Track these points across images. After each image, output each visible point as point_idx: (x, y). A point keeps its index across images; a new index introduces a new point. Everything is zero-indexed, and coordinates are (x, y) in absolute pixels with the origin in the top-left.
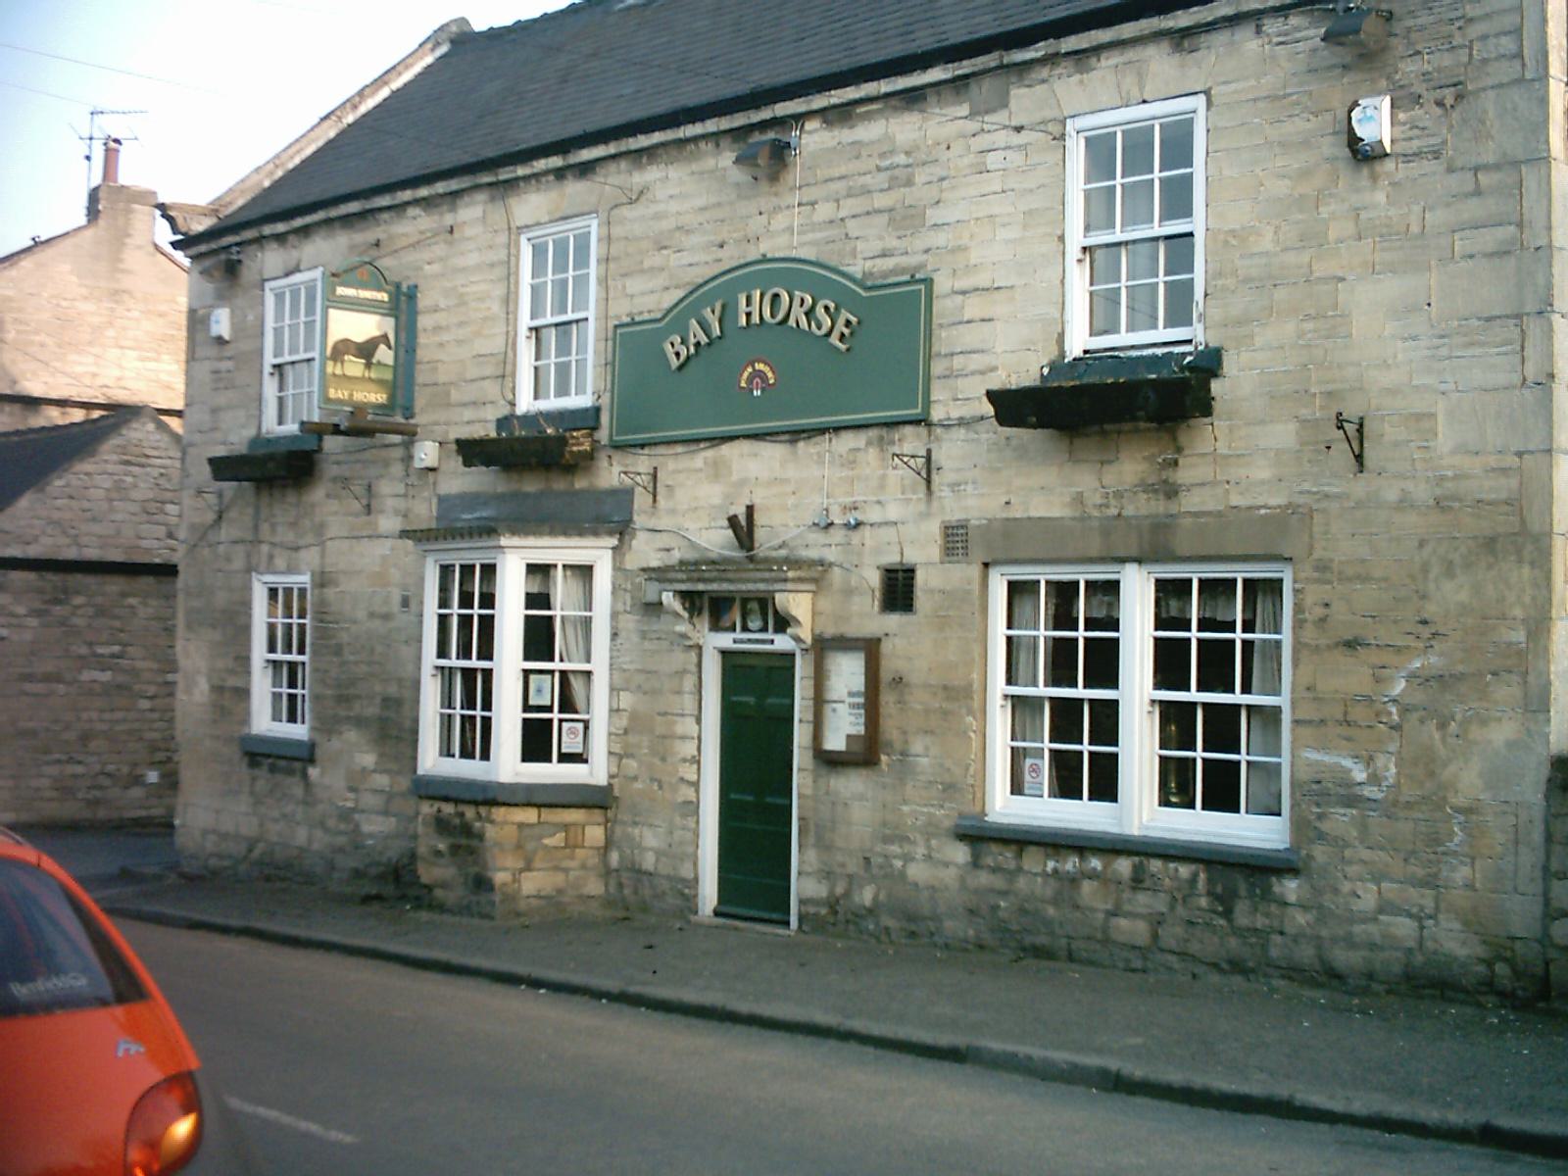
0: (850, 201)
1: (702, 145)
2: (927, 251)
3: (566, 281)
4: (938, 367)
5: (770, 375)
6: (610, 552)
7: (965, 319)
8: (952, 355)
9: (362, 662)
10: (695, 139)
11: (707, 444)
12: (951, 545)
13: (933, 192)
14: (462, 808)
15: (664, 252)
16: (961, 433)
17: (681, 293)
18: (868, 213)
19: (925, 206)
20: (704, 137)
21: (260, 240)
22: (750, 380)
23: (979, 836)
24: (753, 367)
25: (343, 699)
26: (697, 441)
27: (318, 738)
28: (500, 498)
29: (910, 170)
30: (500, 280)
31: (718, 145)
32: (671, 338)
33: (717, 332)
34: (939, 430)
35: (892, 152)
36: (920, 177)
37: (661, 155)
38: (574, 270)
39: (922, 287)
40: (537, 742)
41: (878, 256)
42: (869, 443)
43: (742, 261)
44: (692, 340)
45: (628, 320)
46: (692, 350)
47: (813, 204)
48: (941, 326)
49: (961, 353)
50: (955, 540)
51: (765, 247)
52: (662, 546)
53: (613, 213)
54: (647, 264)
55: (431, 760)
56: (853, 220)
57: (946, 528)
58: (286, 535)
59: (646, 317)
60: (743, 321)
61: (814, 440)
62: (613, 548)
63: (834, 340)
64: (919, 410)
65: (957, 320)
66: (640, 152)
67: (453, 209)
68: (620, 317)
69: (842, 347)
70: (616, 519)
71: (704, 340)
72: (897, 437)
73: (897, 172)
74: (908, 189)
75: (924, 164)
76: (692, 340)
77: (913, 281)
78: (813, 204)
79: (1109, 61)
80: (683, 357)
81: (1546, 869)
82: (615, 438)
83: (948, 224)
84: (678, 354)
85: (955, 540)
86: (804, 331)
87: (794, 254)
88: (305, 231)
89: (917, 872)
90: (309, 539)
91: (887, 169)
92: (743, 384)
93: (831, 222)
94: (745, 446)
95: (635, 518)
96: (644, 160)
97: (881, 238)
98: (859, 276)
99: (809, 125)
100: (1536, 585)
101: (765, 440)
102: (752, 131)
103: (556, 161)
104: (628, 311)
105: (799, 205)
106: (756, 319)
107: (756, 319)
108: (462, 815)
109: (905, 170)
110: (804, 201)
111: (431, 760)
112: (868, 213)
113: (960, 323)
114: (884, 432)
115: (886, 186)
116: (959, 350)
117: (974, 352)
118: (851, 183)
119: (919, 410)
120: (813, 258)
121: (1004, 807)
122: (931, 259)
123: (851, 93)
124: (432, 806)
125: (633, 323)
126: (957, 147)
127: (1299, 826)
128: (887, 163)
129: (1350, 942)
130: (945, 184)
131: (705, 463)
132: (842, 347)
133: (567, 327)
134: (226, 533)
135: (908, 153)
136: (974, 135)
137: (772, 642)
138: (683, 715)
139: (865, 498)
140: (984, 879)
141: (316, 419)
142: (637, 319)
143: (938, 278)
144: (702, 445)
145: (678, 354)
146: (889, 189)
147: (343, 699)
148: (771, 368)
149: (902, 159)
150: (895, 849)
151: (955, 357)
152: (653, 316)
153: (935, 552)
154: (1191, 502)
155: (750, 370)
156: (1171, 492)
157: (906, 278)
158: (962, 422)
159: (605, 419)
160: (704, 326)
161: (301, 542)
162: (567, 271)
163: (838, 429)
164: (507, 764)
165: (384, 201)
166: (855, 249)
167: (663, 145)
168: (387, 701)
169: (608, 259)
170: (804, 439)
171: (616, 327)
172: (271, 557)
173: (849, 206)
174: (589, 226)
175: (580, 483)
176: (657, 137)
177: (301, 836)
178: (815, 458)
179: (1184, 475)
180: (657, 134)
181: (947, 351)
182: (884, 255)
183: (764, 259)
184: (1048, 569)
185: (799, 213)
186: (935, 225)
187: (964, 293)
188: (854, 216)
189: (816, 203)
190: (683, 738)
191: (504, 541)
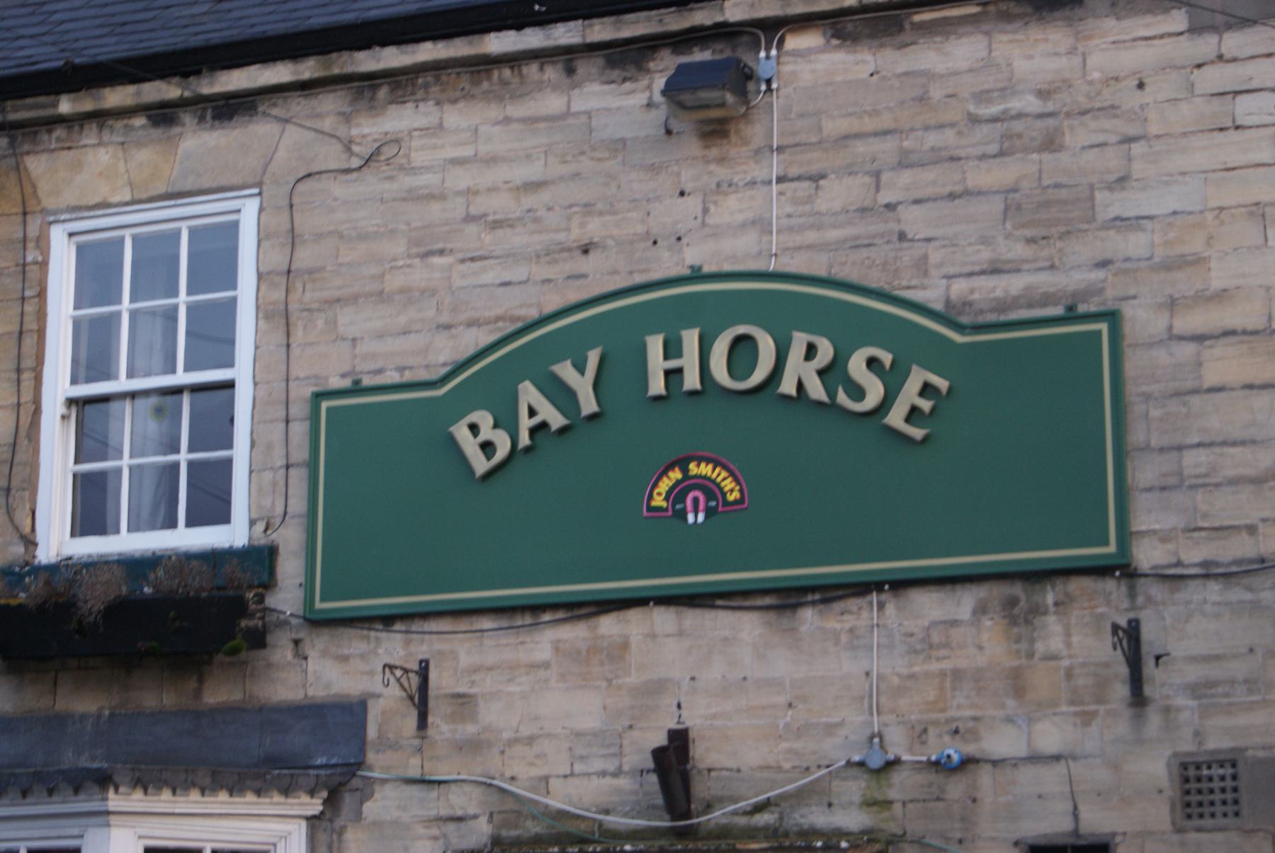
0: (906, 177)
1: (532, 70)
2: (1104, 264)
3: (170, 316)
4: (1144, 472)
5: (728, 484)
6: (304, 824)
7: (1206, 385)
8: (1180, 448)
10: (514, 60)
11: (560, 615)
12: (1194, 798)
13: (1112, 160)
15: (437, 260)
16: (1213, 591)
17: (485, 337)
18: (952, 196)
19: (1092, 187)
20: (540, 56)
22: (676, 495)
24: (685, 471)
26: (536, 608)
29: (1051, 122)
30: (17, 299)
31: (570, 71)
32: (474, 417)
33: (589, 405)
34: (1156, 590)
35: (1007, 90)
36: (1077, 136)
37: (426, 86)
38: (132, 300)
39: (1103, 327)
41: (983, 273)
42: (981, 610)
43: (639, 279)
44: (525, 423)
45: (346, 383)
46: (524, 440)
47: (816, 178)
48: (1147, 397)
49: (1199, 445)
51: (696, 254)
53: (301, 187)
54: (394, 282)
56: (915, 207)
57: (1184, 766)
59: (392, 377)
60: (657, 386)
61: (837, 606)
62: (309, 819)
63: (896, 418)
64: (1112, 548)
65: (1190, 384)
66: (372, 79)
67: (130, 118)
68: (326, 378)
69: (917, 433)
70: (320, 761)
71: (556, 420)
72: (1050, 598)
73: (1018, 126)
74: (1046, 157)
75: (1084, 113)
76: (525, 423)
77: (1071, 316)
78: (816, 178)
80: (502, 452)
82: (319, 605)
83: (1150, 218)
84: (487, 447)
86: (820, 404)
87: (772, 266)
91: (995, 120)
92: (658, 501)
93: (863, 210)
94: (663, 618)
95: (371, 757)
96: (383, 93)
97: (985, 241)
98: (938, 306)
99: (794, 42)
101: (713, 607)
102: (655, 49)
103: (169, 90)
104: (346, 368)
105: (770, 182)
106: (692, 380)
107: (692, 380)
109: (1040, 124)
110: (794, 171)
112: (952, 196)
113: (1195, 391)
114: (1017, 589)
115: (993, 148)
116: (1196, 440)
117: (1234, 444)
118: (906, 144)
119: (1112, 548)
120: (822, 272)
122: (1110, 278)
125: (357, 389)
126: (1160, 89)
128: (995, 109)
130: (1137, 148)
131: (557, 650)
132: (917, 433)
133: (101, 406)
135: (1043, 94)
136: (1199, 66)
139: (972, 713)
142: (367, 381)
143: (1128, 311)
144: (547, 617)
145: (487, 448)
146: (1001, 154)
148: (732, 474)
149: (1031, 103)
151: (1185, 452)
152: (424, 375)
153: (1159, 814)
155: (676, 475)
157: (1058, 311)
158: (1209, 572)
159: (290, 569)
160: (562, 395)
162: (175, 293)
163: (901, 584)
166: (925, 257)
167: (436, 67)
169: (289, 272)
170: (813, 603)
171: (319, 396)
173: (897, 186)
174: (239, 211)
175: (218, 693)
176: (427, 52)
178: (844, 638)
180: (428, 45)
181: (1165, 441)
182: (995, 269)
183: (697, 275)
185: (780, 193)
186: (1117, 218)
187: (1199, 338)
188: (917, 202)
189: (823, 176)
191: (115, 801)
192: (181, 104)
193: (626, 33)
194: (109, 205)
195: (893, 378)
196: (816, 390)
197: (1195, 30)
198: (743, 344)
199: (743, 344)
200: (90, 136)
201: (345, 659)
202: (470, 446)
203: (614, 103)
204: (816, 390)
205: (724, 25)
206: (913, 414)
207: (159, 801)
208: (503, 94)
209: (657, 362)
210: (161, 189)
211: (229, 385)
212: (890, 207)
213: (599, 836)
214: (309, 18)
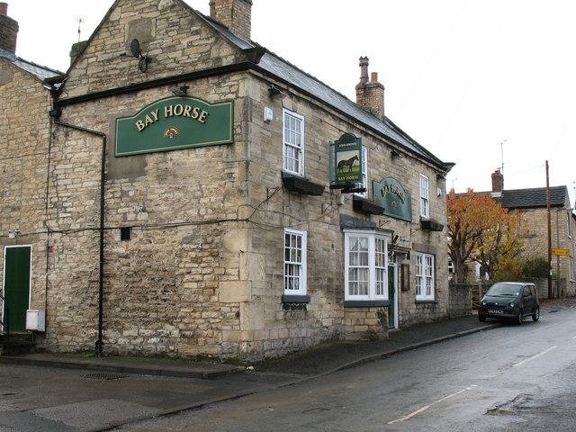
23: (417, 303)
25: (317, 279)
55: (348, 297)
58: (295, 214)
60: (166, 115)
63: (200, 119)
71: (152, 121)
79: (430, 170)
100: (509, 268)
103: (364, 129)
106: (171, 114)
107: (171, 114)
134: (271, 207)
141: (300, 173)
145: (141, 126)
147: (317, 279)
160: (152, 117)
165: (328, 109)
172: (290, 222)
177: (304, 333)
195: (199, 112)
196: (189, 115)
198: (178, 107)
199: (178, 107)
202: (138, 126)
204: (189, 115)
206: (203, 119)
207: (20, 363)
209: (166, 111)
211: (356, 294)
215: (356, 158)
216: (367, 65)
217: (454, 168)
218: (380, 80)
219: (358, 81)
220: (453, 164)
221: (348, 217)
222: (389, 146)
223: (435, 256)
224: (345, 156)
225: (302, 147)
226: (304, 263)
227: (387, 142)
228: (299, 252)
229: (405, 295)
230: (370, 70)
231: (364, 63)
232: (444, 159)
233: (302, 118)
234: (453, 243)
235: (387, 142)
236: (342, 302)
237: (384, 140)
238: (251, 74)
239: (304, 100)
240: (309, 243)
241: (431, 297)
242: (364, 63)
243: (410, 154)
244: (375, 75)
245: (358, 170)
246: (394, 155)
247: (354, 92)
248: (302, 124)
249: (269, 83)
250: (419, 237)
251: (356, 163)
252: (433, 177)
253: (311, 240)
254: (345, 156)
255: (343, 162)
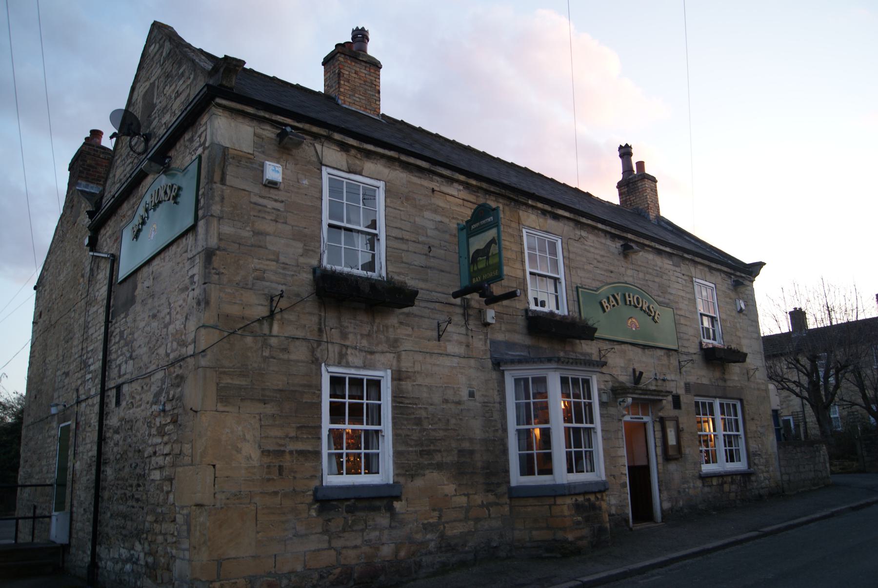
9: (439, 429)
14: (587, 497)
21: (329, 139)
23: (705, 478)
27: (402, 480)
28: (528, 347)
40: (575, 463)
50: (688, 387)
52: (605, 380)
55: (516, 478)
59: (587, 287)
79: (700, 267)
81: (780, 465)
85: (688, 387)
88: (369, 154)
89: (691, 492)
90: (383, 347)
103: (548, 208)
107: (632, 303)
108: (589, 500)
111: (516, 478)
121: (333, 480)
123: (647, 242)
124: (572, 499)
127: (750, 462)
129: (762, 488)
135: (660, 268)
137: (642, 419)
138: (619, 447)
140: (706, 489)
142: (584, 287)
150: (686, 486)
154: (729, 384)
156: (725, 380)
161: (374, 349)
164: (561, 475)
168: (461, 452)
176: (589, 222)
179: (727, 377)
184: (702, 398)
190: (621, 457)
192: (550, 212)
193: (616, 233)
194: (535, 229)
197: (673, 265)
200: (530, 211)
201: (587, 345)
203: (610, 244)
205: (627, 238)
208: (597, 236)
210: (545, 229)
212: (647, 280)
213: (541, 381)
214: (184, 82)
215: (493, 241)
216: (630, 154)
217: (763, 271)
218: (648, 170)
219: (620, 177)
220: (760, 265)
221: (510, 345)
222: (614, 237)
223: (741, 400)
224: (478, 243)
225: (381, 230)
226: (387, 425)
227: (608, 229)
228: (736, 421)
229: (672, 467)
230: (634, 160)
231: (625, 152)
232: (748, 259)
233: (381, 184)
234: (810, 383)
235: (608, 229)
236: (503, 489)
237: (600, 226)
238: (225, 108)
239: (383, 156)
240: (397, 397)
241: (740, 465)
242: (625, 152)
243: (668, 250)
244: (641, 165)
245: (496, 260)
246: (626, 250)
247: (616, 192)
248: (381, 196)
249: (274, 124)
250: (700, 375)
251: (494, 249)
252: (725, 284)
253: (407, 385)
254: (478, 243)
255: (478, 252)
